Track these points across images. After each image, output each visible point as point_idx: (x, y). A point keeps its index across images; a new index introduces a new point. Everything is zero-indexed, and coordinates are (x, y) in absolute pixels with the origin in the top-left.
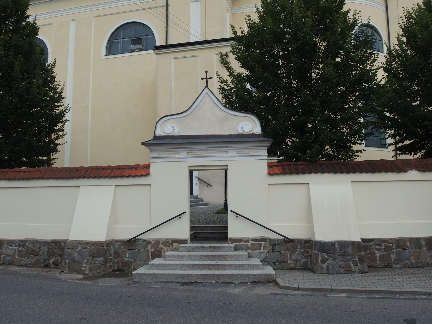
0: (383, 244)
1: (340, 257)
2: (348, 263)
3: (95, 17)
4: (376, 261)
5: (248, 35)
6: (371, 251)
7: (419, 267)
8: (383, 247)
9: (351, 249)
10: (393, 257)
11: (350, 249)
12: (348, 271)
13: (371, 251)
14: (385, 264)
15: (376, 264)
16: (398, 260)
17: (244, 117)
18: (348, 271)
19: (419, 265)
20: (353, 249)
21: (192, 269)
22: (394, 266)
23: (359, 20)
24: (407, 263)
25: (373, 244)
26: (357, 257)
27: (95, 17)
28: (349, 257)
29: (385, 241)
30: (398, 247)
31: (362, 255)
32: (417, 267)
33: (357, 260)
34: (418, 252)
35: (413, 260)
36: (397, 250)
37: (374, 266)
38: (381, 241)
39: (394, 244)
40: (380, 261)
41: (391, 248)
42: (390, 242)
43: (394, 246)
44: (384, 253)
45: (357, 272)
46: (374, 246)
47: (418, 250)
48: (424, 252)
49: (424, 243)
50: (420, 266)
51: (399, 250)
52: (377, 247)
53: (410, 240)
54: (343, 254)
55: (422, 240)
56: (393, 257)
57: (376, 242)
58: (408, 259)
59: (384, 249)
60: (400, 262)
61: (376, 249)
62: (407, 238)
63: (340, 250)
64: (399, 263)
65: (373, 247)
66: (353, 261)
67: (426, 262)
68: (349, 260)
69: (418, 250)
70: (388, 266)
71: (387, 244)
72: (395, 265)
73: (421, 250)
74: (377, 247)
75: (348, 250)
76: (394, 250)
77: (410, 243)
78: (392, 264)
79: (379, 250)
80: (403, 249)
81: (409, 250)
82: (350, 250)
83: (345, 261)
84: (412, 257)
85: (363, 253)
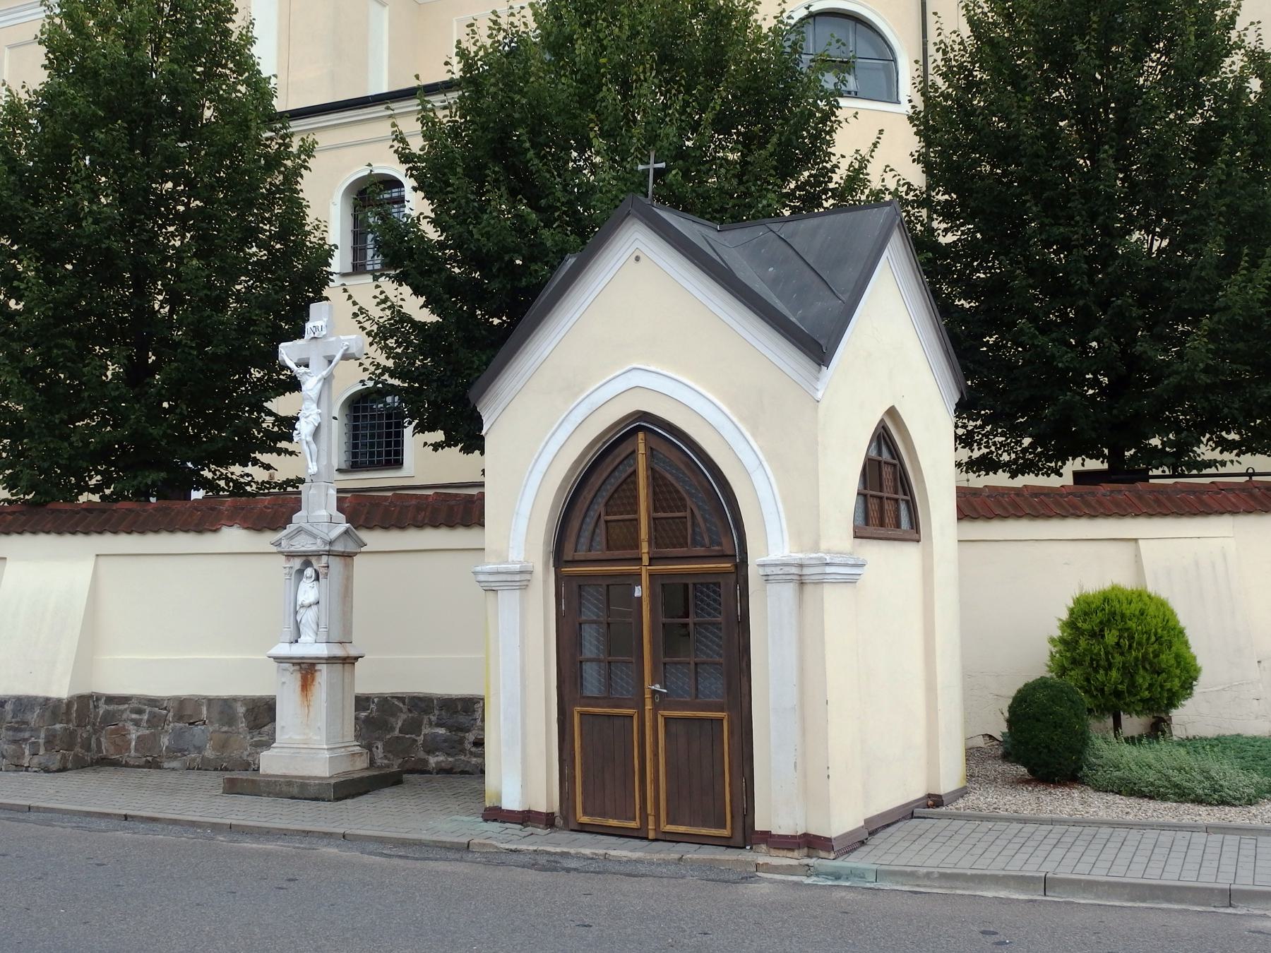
0: (148, 709)
1: (11, 733)
2: (21, 747)
3: (10, 47)
4: (128, 749)
5: (234, 95)
6: (121, 725)
7: (221, 770)
8: (146, 717)
9: (38, 716)
10: (165, 741)
11: (35, 716)
12: (16, 766)
13: (121, 725)
14: (148, 758)
15: (128, 756)
16: (177, 751)
17: (660, 395)
18: (16, 766)
19: (225, 764)
20: (41, 716)
21: (1007, 887)
22: (166, 765)
23: (525, 24)
24: (194, 760)
25: (126, 709)
26: (42, 735)
27: (10, 47)
28: (27, 735)
29: (153, 702)
30: (179, 717)
31: (55, 730)
32: (216, 769)
33: (41, 741)
34: (225, 732)
35: (209, 753)
36: (176, 724)
37: (124, 762)
38: (146, 702)
39: (172, 710)
40: (136, 750)
41: (164, 719)
42: (165, 705)
43: (171, 714)
44: (148, 732)
45: (34, 769)
46: (128, 712)
47: (225, 729)
48: (239, 733)
49: (241, 710)
50: (225, 767)
51: (181, 725)
52: (134, 716)
53: (210, 701)
54: (16, 726)
55: (239, 704)
56: (165, 741)
57: (134, 705)
58: (199, 749)
59: (148, 721)
60: (179, 754)
61: (132, 720)
62: (205, 698)
63: (13, 717)
64: (177, 757)
65: (125, 716)
66: (33, 743)
67: (241, 757)
68: (25, 740)
69: (225, 729)
70: (154, 764)
71: (157, 709)
72: (169, 762)
73: (234, 728)
74: (134, 716)
75: (29, 718)
76: (168, 725)
77: (208, 710)
78: (164, 760)
79: (137, 723)
80: (190, 724)
81: (203, 727)
82: (33, 717)
83: (15, 742)
84: (208, 745)
85: (58, 726)
